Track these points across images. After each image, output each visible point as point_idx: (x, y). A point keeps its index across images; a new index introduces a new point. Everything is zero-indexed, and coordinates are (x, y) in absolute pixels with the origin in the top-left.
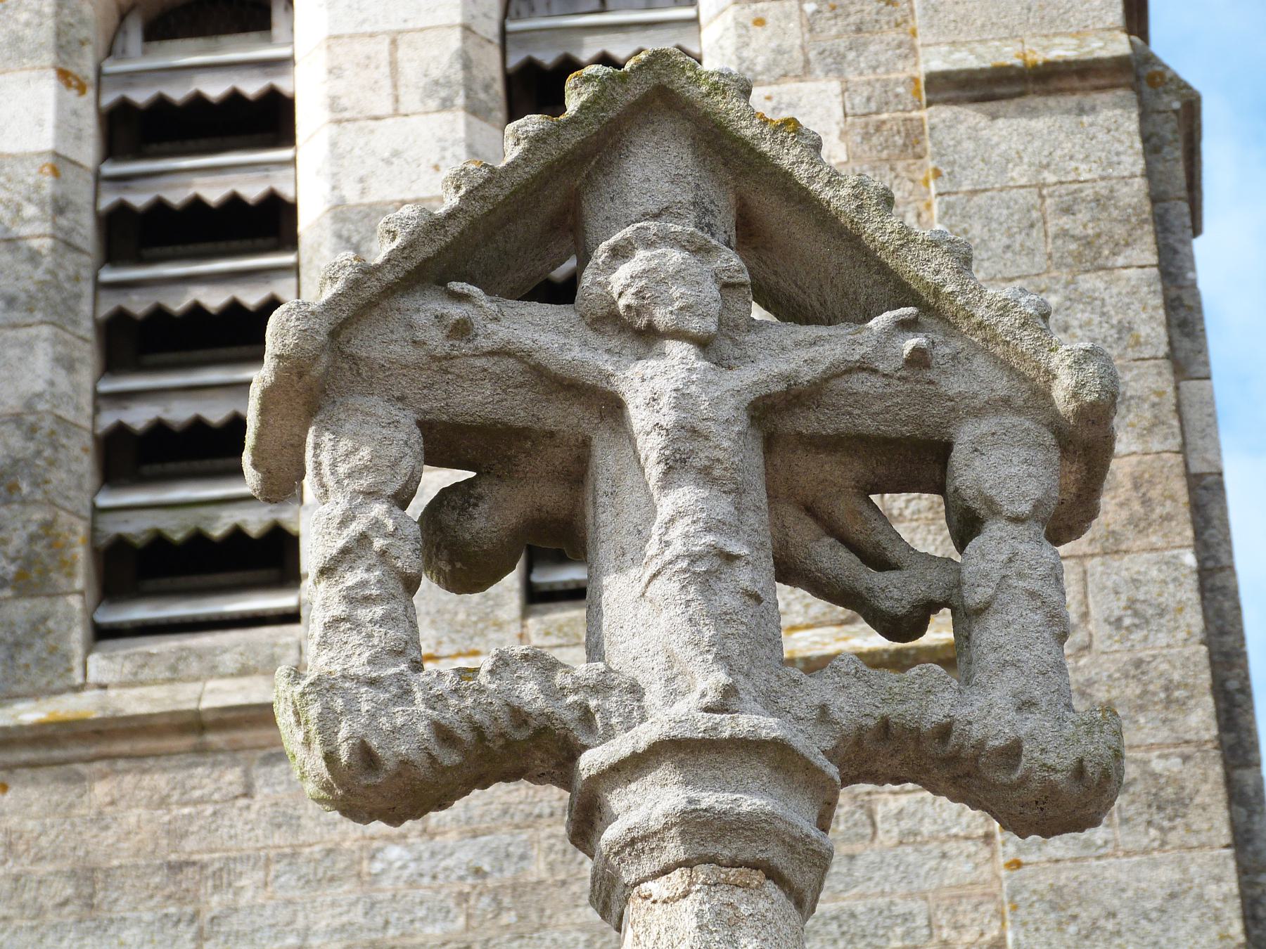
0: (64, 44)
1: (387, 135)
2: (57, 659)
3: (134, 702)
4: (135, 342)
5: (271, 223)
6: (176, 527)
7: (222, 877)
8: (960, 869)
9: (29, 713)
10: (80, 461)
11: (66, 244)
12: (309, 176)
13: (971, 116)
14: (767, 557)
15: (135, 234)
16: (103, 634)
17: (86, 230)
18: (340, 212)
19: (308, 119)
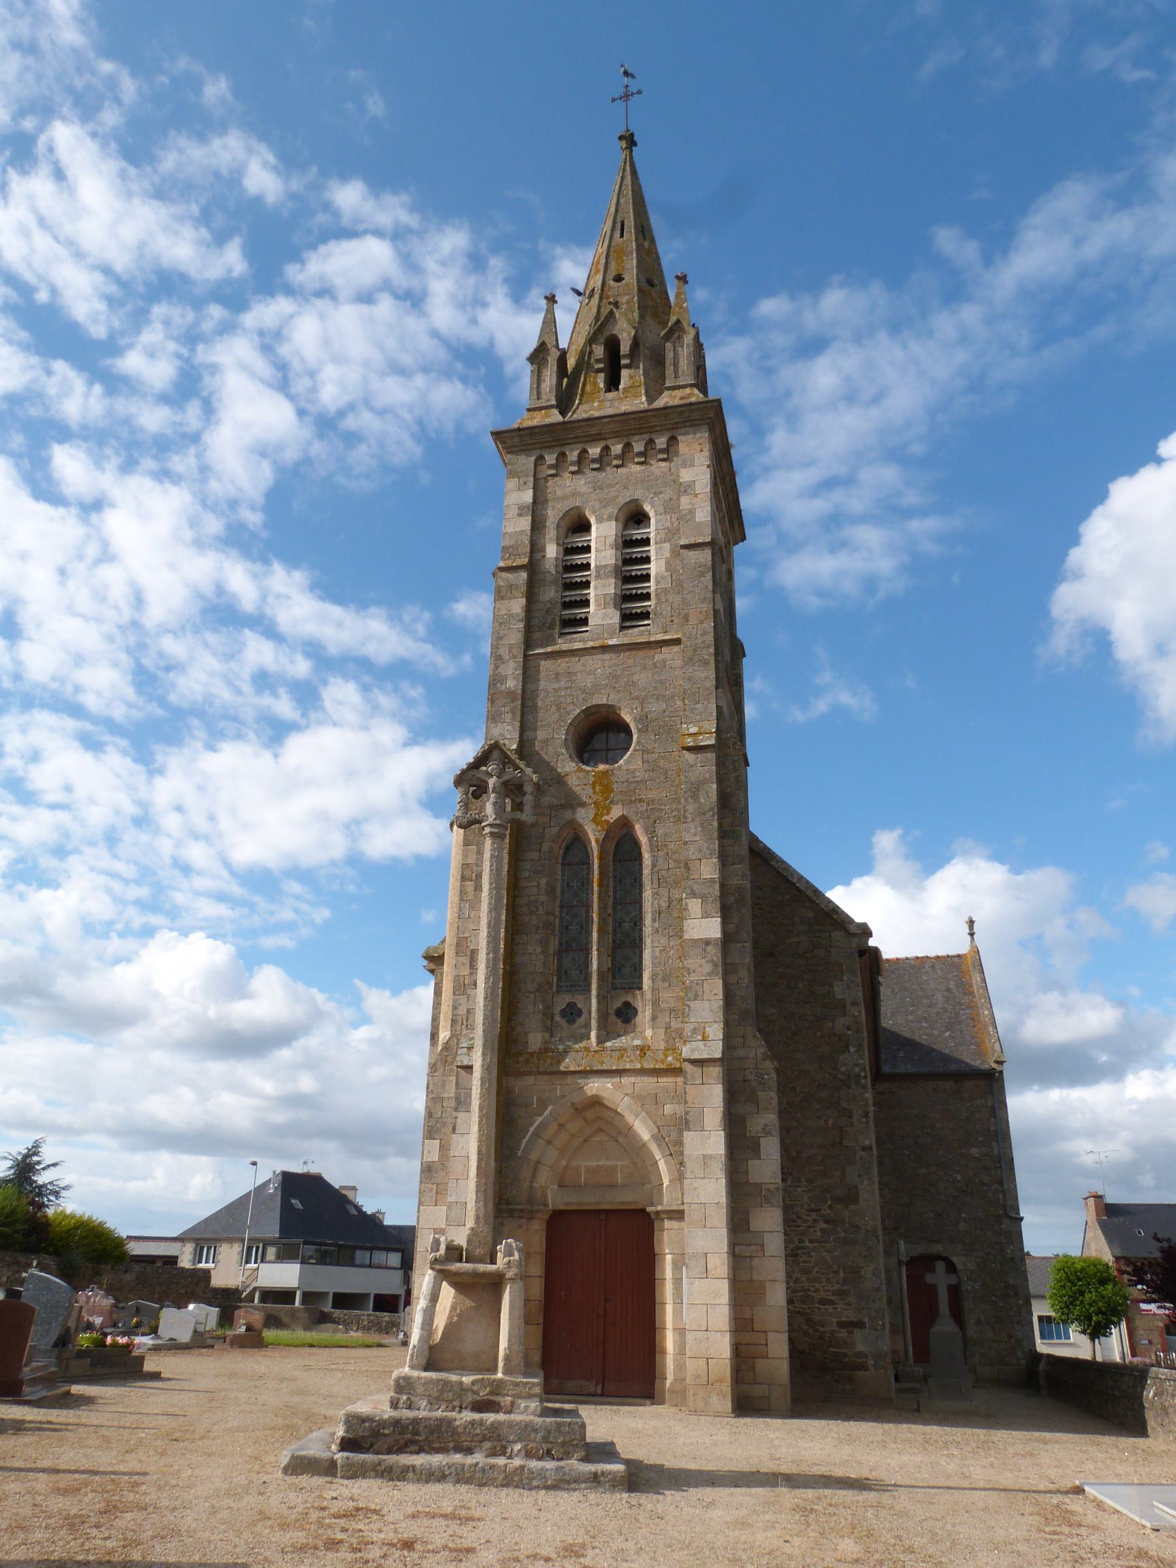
0: (558, 539)
1: (604, 553)
2: (554, 640)
3: (564, 647)
4: (627, 579)
5: (587, 567)
6: (572, 617)
7: (575, 674)
8: (677, 673)
9: (549, 649)
10: (559, 606)
11: (557, 572)
12: (593, 558)
13: (686, 551)
14: (23, 730)
15: (628, 561)
16: (562, 634)
17: (560, 569)
18: (596, 566)
19: (593, 550)
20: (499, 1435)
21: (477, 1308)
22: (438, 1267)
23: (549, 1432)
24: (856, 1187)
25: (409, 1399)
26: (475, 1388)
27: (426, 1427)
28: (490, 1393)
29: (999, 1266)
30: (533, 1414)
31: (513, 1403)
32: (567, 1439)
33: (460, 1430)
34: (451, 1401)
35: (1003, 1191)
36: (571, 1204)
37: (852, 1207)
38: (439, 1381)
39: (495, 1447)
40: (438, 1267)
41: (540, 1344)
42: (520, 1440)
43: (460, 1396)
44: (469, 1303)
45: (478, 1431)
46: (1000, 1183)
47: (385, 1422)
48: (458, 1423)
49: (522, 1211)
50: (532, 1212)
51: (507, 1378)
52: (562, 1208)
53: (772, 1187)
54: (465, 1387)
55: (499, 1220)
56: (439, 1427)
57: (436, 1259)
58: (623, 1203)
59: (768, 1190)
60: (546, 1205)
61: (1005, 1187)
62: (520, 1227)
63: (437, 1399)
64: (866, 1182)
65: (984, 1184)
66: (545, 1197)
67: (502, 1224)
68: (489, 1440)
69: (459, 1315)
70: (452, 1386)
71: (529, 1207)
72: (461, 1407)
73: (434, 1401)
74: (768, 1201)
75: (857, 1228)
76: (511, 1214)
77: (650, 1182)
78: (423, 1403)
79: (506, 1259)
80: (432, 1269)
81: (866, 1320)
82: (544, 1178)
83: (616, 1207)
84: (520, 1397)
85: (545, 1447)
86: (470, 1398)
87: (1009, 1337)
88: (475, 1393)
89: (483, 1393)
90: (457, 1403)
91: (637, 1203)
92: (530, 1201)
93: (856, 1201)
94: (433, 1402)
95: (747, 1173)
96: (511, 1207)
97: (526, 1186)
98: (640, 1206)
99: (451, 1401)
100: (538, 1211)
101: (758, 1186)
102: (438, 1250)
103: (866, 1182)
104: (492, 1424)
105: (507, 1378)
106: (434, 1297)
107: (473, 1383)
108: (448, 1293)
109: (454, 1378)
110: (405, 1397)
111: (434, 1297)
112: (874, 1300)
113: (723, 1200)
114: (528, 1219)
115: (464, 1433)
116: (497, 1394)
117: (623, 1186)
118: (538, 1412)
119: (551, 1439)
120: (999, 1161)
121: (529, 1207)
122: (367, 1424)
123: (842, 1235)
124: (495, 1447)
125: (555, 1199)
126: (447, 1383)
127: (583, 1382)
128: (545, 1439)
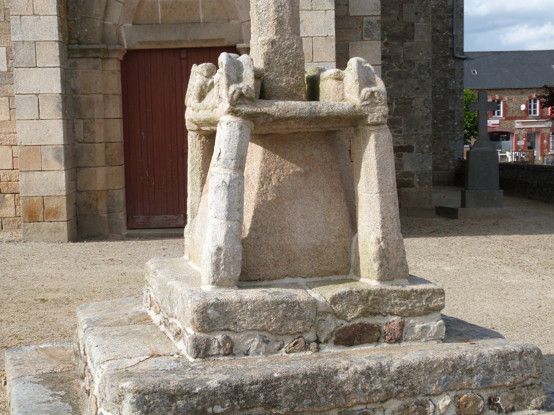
20: (412, 388)
21: (305, 174)
22: (246, 109)
23: (491, 371)
24: (413, 25)
25: (227, 339)
26: (338, 308)
27: (288, 391)
28: (364, 314)
29: (442, 96)
30: (437, 338)
31: (402, 325)
32: (519, 378)
33: (348, 388)
34: (300, 334)
35: (453, 37)
36: (149, 43)
37: (407, 43)
38: (277, 303)
39: (407, 407)
40: (246, 109)
41: (123, 184)
42: (446, 390)
43: (315, 325)
44: (291, 168)
45: (378, 386)
46: (451, 30)
47: (214, 393)
48: (342, 377)
49: (99, 50)
50: (108, 51)
51: (388, 287)
52: (138, 47)
53: (373, 20)
54: (321, 308)
55: (72, 61)
56: (312, 387)
57: (241, 95)
58: (207, 41)
59: (370, 23)
60: (120, 43)
61: (455, 33)
62: (96, 68)
63: (277, 333)
64: (422, 20)
65: (437, 31)
66: (119, 35)
67: (75, 65)
68: (397, 396)
69: (278, 189)
70: (301, 310)
71: (104, 46)
72: (318, 341)
73: (269, 337)
74: (369, 35)
75: (411, 63)
76: (84, 54)
77: (236, 18)
78: (254, 343)
79: (366, 91)
80: (233, 112)
81: (414, 145)
82: (116, 14)
83: (199, 45)
84: (412, 314)
85: (485, 394)
86: (331, 325)
87: (444, 149)
88: (338, 316)
89: (353, 316)
90: (310, 336)
91: (223, 39)
92: (103, 40)
93: (412, 38)
94: (271, 339)
95: (347, 5)
96: (84, 46)
97: (98, 24)
98: (232, 44)
99: (300, 334)
100: (114, 51)
101: (359, 18)
102: (239, 80)
103: (422, 20)
104: (400, 371)
105: (388, 287)
106: (240, 163)
107: (335, 300)
108: (256, 153)
109: (301, 295)
110: (219, 337)
111: (240, 163)
112: (422, 127)
113: (333, 33)
114: (104, 59)
115: (355, 391)
116: (375, 314)
117: (206, 23)
118: (443, 335)
119: (495, 383)
120: (452, 10)
121: (104, 46)
122: (180, 403)
123: (397, 69)
124: (407, 407)
125: (130, 37)
126: (292, 306)
127: (170, 216)
128: (485, 383)
